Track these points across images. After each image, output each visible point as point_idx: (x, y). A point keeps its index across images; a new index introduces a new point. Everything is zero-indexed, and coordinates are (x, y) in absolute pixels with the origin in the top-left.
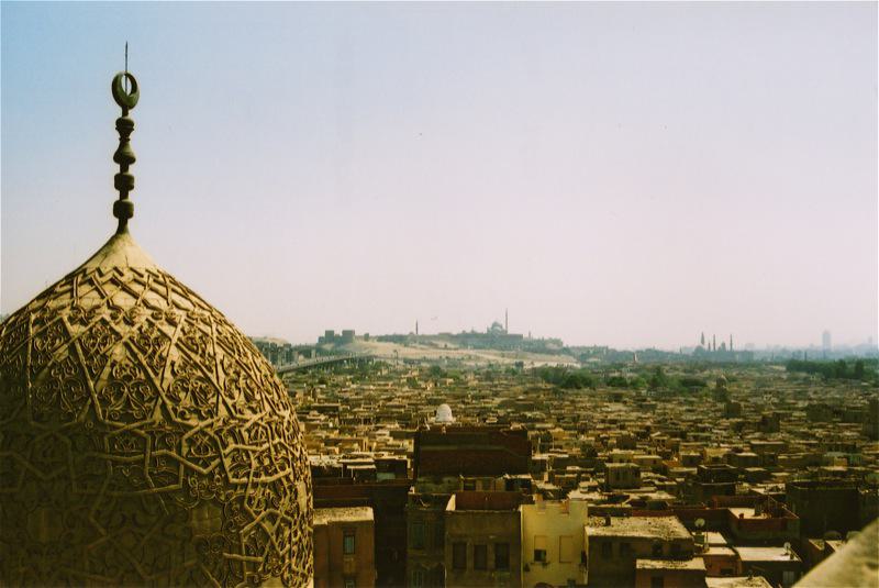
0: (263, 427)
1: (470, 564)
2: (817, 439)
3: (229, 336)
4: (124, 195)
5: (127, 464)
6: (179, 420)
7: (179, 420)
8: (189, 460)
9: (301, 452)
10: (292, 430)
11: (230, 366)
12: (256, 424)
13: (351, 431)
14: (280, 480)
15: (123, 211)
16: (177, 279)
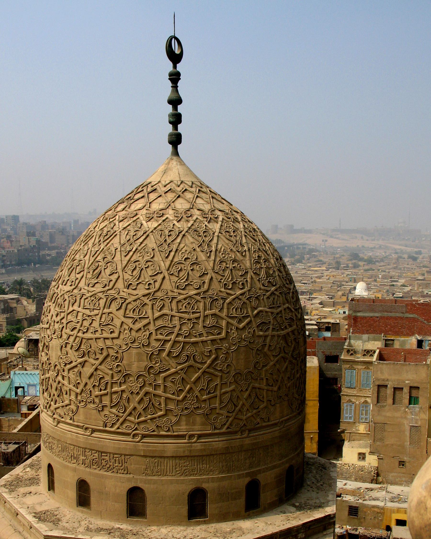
4: (175, 128)
14: (288, 334)
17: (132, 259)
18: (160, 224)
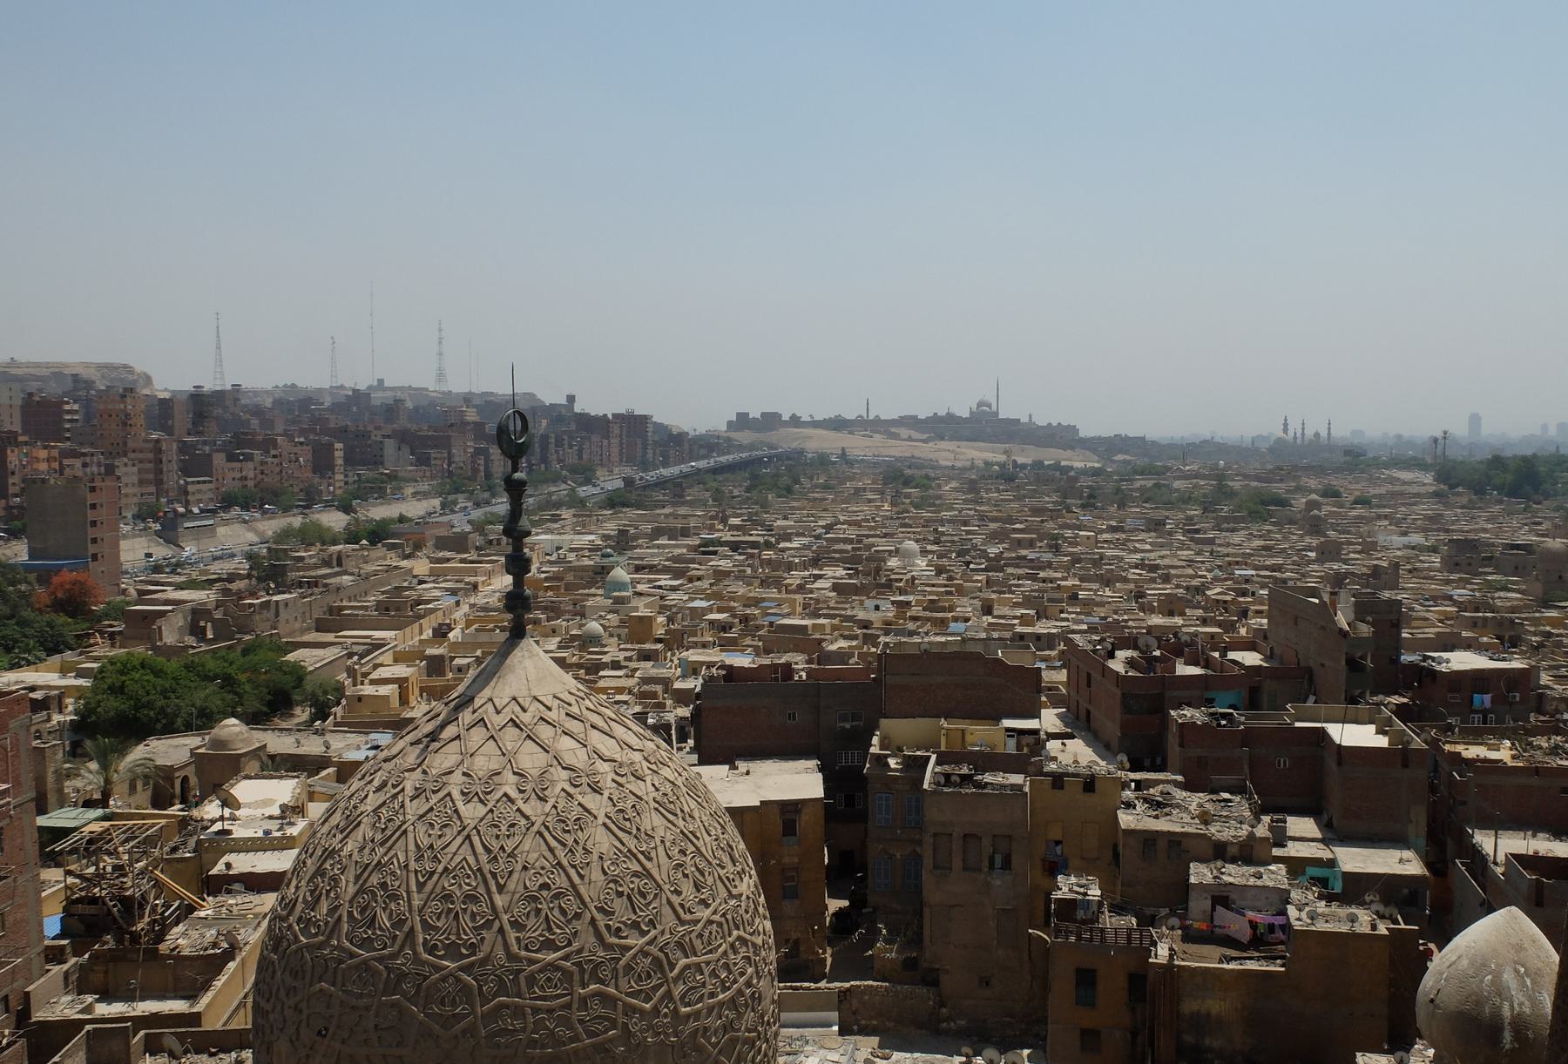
1: (957, 863)
2: (1454, 603)
5: (550, 1011)
8: (628, 994)
13: (778, 583)
17: (438, 890)
18: (491, 811)
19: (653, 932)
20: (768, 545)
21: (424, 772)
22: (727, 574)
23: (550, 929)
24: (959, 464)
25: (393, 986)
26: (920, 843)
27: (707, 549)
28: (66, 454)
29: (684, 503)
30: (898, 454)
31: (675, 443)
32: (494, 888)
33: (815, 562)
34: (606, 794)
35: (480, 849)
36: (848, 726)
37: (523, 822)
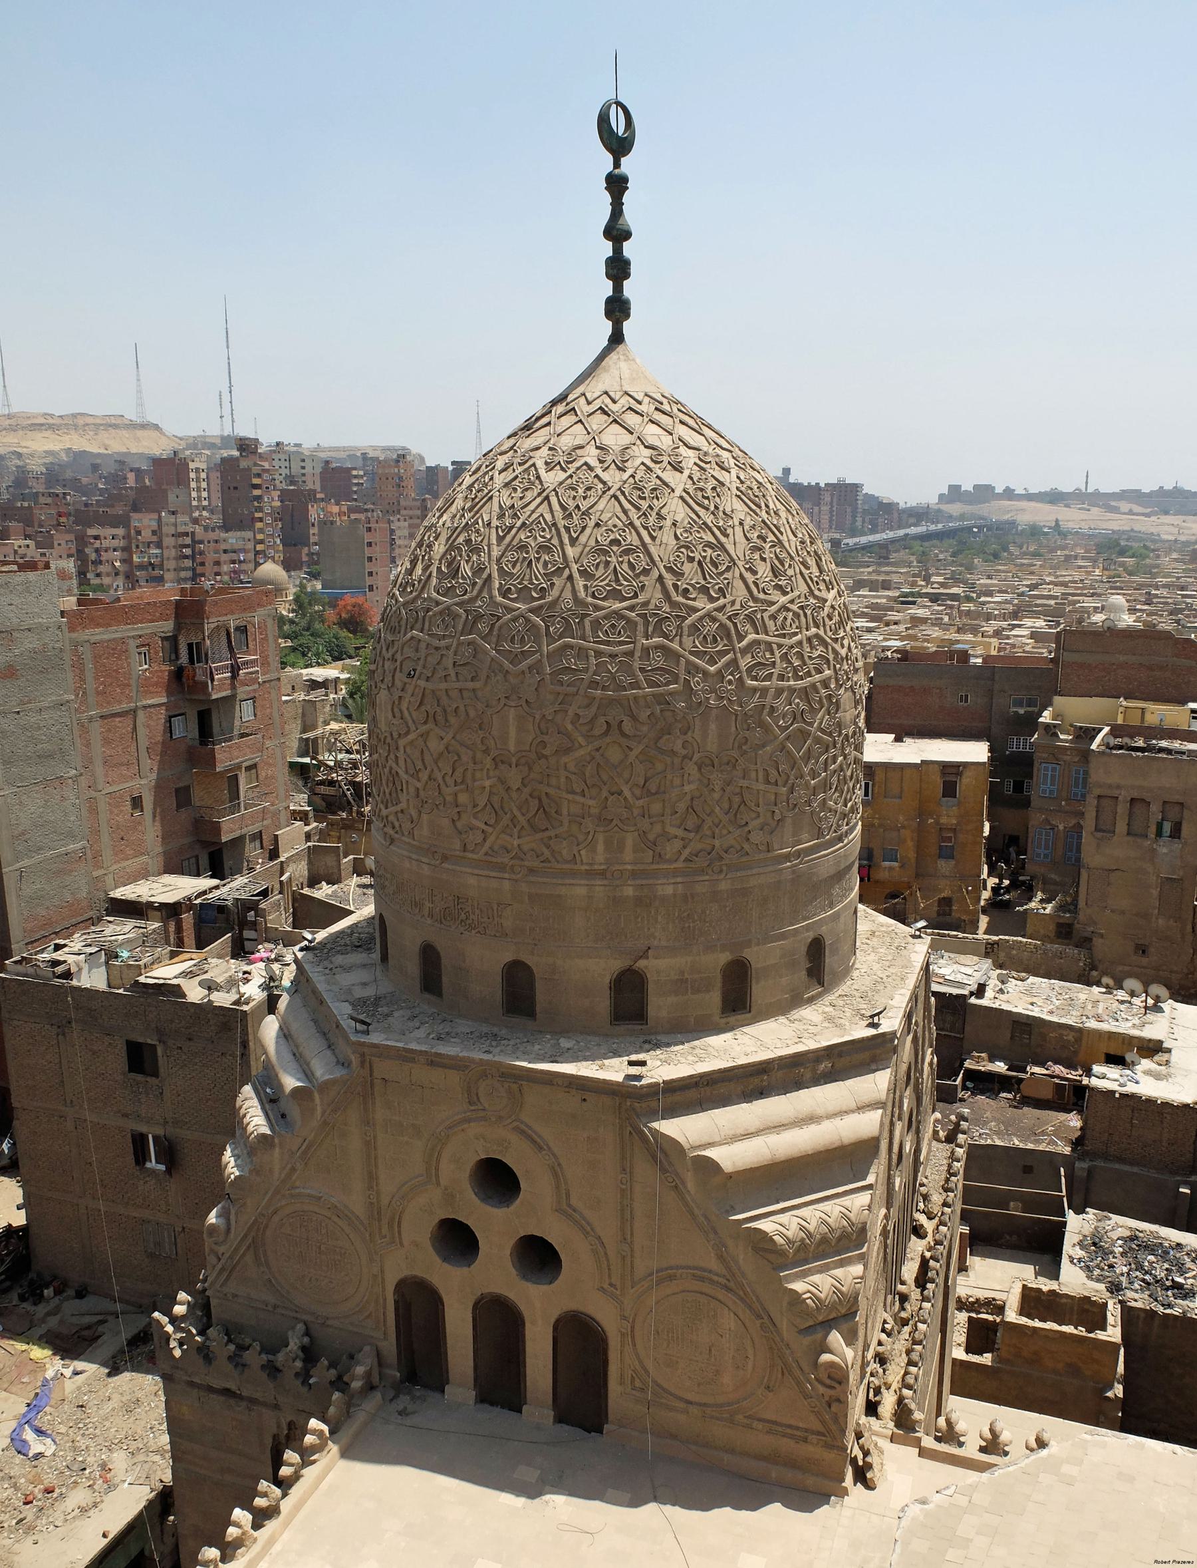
0: (795, 613)
1: (1121, 827)
3: (755, 486)
5: (613, 656)
6: (681, 599)
7: (681, 599)
8: (691, 653)
9: (849, 648)
10: (836, 618)
11: (753, 527)
12: (785, 608)
13: (974, 630)
14: (813, 686)
15: (617, 308)
16: (692, 406)
17: (514, 543)
18: (571, 476)
19: (722, 601)
20: (969, 599)
21: (516, 451)
22: (924, 621)
23: (617, 580)
24: (1183, 538)
25: (470, 627)
26: (1082, 814)
27: (907, 601)
28: (351, 510)
29: (888, 565)
30: (1116, 528)
31: (884, 512)
32: (566, 541)
33: (1015, 615)
34: (686, 473)
35: (556, 506)
36: (1021, 711)
37: (600, 486)
